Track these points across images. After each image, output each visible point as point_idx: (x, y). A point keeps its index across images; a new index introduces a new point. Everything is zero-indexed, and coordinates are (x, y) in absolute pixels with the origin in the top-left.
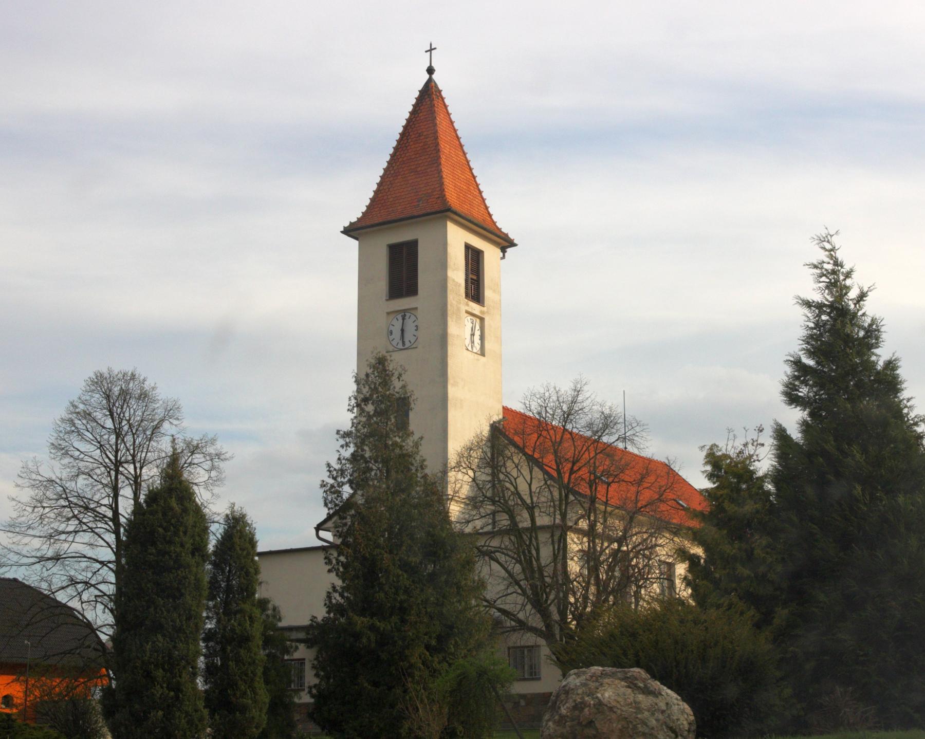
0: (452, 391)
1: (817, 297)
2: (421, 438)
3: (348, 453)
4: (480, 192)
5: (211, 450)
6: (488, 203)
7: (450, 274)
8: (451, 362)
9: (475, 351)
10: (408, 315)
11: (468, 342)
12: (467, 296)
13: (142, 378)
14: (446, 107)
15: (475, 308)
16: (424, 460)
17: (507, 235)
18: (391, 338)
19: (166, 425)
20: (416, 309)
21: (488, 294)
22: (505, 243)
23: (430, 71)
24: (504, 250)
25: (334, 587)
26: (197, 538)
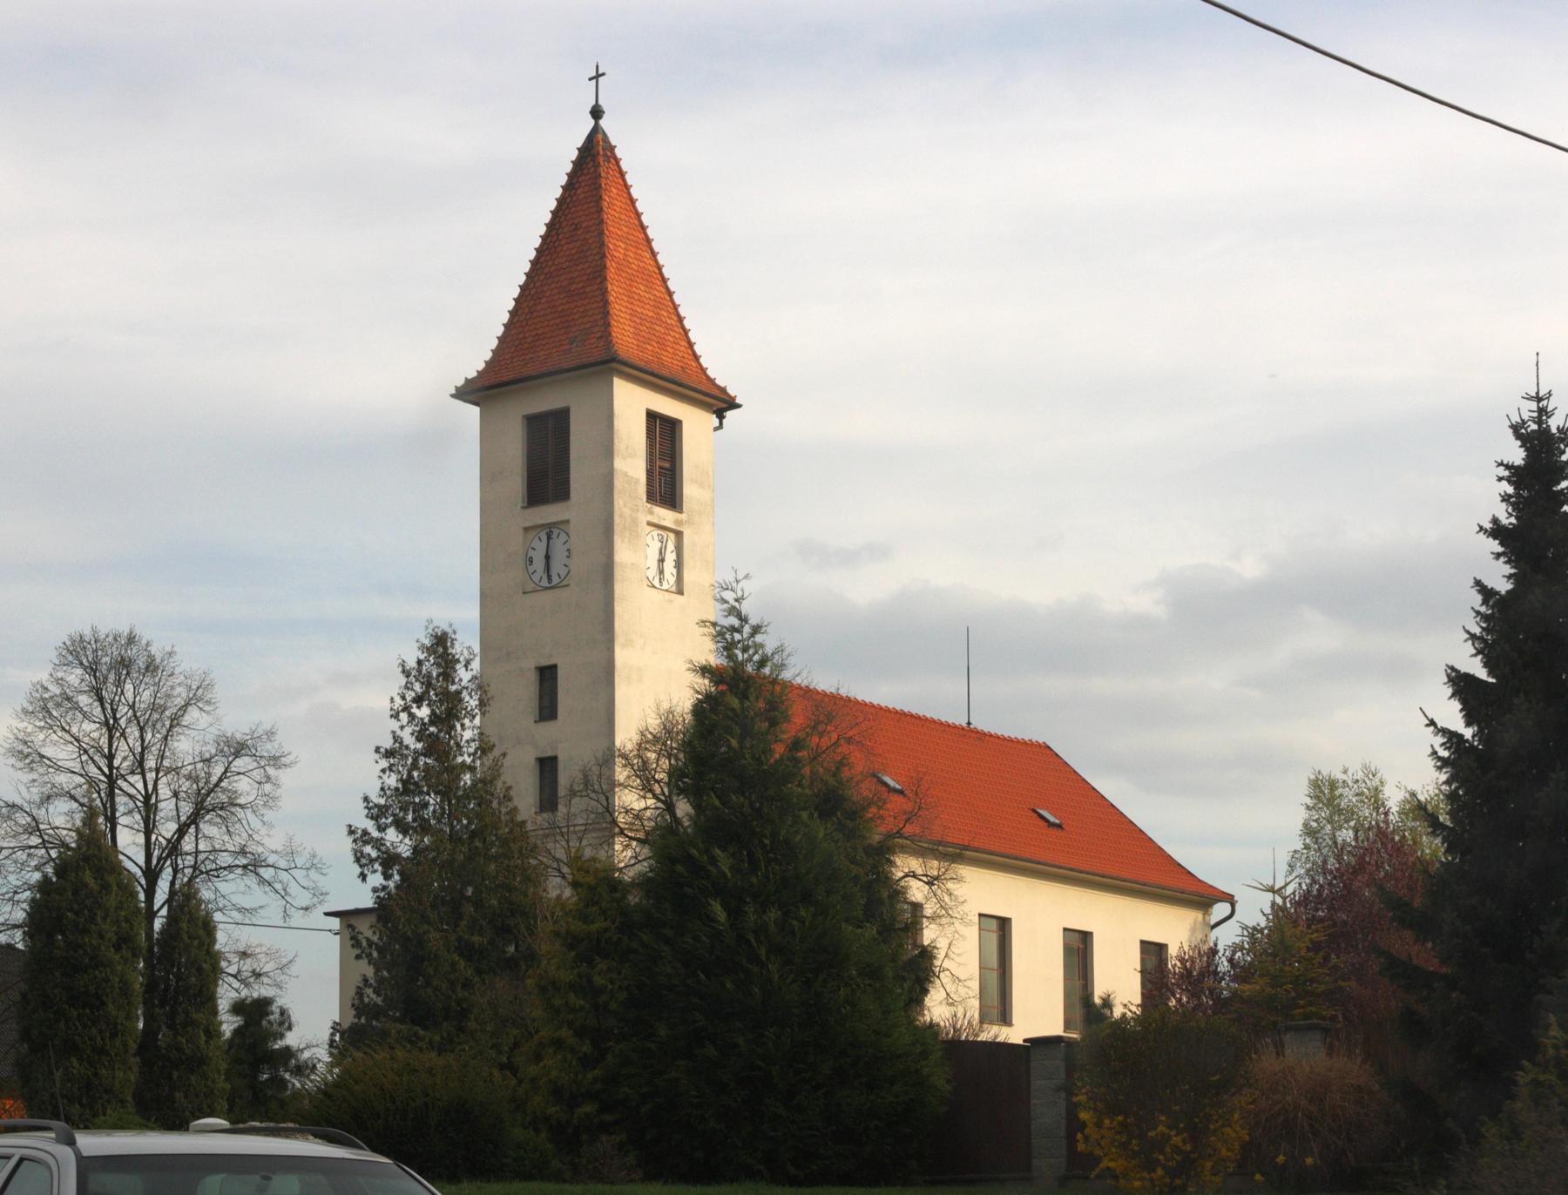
0: (621, 655)
1: (715, 660)
2: (504, 755)
3: (392, 781)
4: (680, 319)
5: (267, 749)
6: (693, 336)
7: (619, 464)
8: (619, 609)
9: (665, 586)
10: (556, 532)
11: (653, 573)
12: (651, 497)
13: (144, 642)
14: (622, 174)
15: (666, 516)
16: (510, 788)
17: (723, 390)
18: (531, 569)
19: (193, 714)
20: (568, 521)
21: (690, 490)
22: (721, 404)
23: (597, 113)
24: (720, 415)
25: (366, 980)
26: (123, 924)
